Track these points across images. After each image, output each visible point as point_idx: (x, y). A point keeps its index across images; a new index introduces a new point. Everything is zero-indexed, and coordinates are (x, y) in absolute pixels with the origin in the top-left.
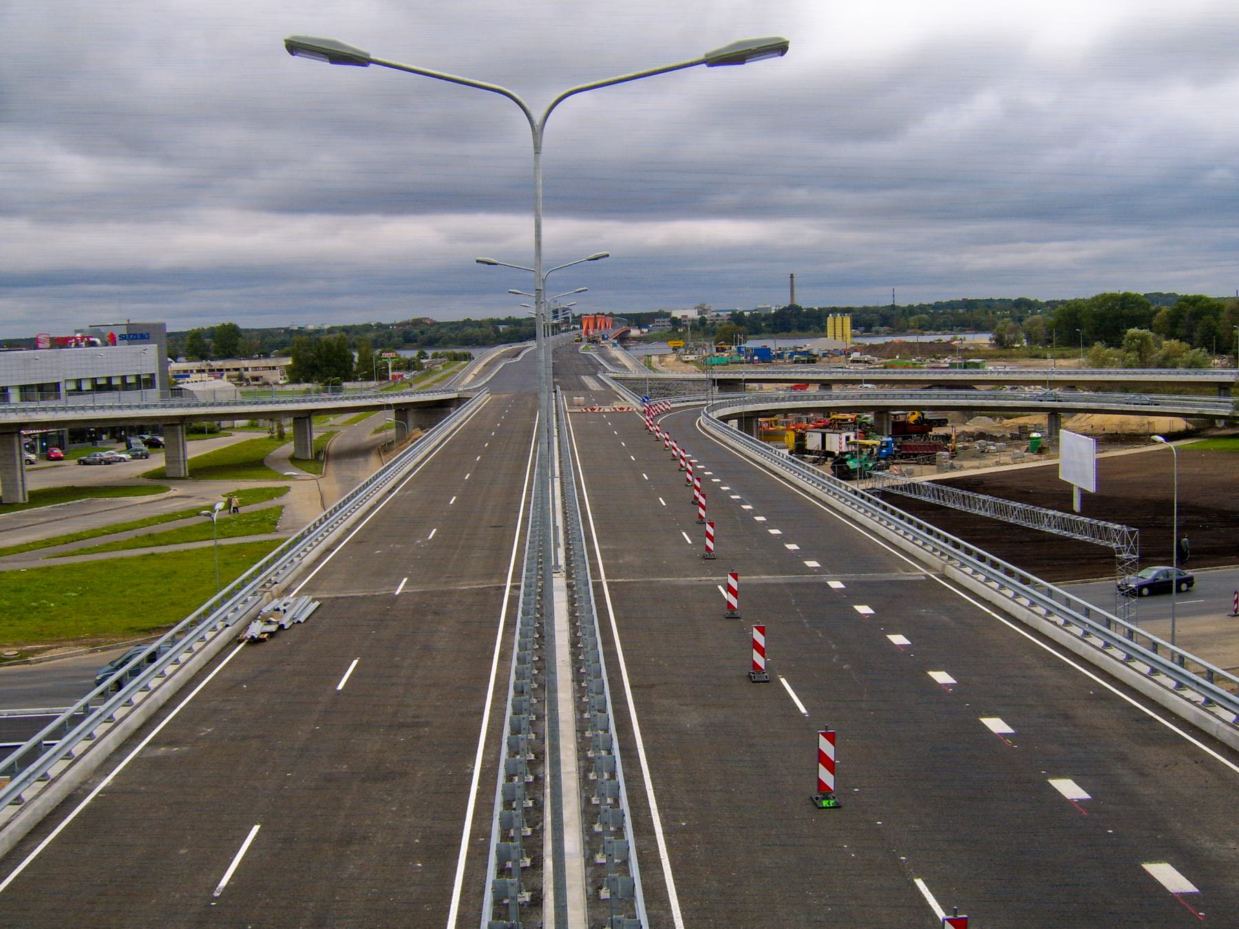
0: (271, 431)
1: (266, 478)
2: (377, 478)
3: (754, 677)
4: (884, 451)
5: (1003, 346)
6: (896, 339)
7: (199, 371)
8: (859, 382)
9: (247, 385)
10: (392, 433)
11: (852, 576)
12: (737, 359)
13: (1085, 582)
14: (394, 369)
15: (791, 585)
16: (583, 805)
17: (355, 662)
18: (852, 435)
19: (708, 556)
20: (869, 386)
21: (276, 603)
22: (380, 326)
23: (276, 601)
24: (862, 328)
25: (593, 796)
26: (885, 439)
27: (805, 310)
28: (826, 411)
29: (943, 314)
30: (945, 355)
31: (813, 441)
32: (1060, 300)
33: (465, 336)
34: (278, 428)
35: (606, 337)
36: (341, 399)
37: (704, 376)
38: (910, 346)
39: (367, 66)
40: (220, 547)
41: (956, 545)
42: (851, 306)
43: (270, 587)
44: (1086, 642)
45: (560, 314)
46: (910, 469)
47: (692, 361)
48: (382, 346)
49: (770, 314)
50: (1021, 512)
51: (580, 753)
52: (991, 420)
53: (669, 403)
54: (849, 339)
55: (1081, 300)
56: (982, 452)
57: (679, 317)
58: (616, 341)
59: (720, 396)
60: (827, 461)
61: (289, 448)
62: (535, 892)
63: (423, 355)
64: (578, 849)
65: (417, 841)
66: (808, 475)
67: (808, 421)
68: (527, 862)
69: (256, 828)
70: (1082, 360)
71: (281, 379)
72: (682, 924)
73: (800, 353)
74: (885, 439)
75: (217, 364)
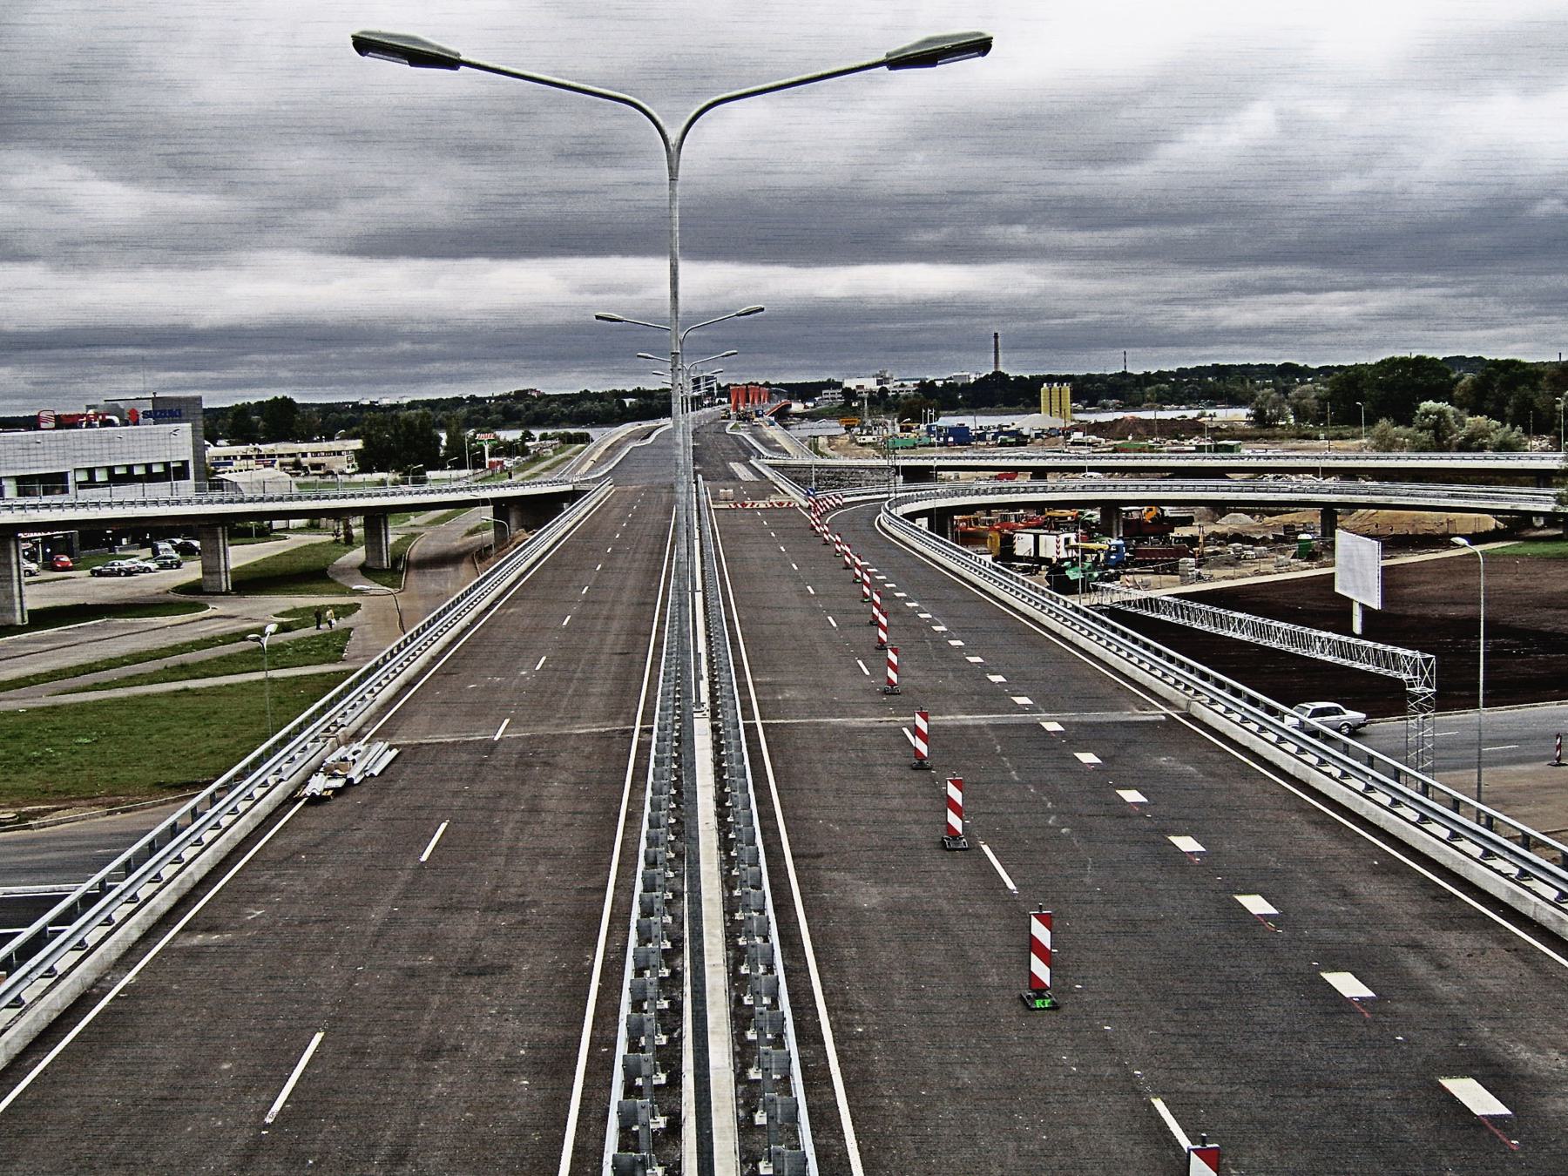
0: (336, 533)
4: (1113, 557)
5: (1264, 427)
7: (244, 457)
8: (1081, 469)
10: (491, 533)
12: (926, 440)
14: (491, 455)
15: (995, 727)
18: (1072, 536)
19: (890, 690)
21: (342, 751)
23: (343, 748)
31: (1023, 545)
35: (760, 413)
40: (272, 680)
41: (1204, 676)
43: (336, 731)
47: (869, 443)
57: (853, 388)
59: (904, 488)
61: (358, 554)
65: (522, 1052)
68: (662, 1078)
73: (1006, 433)
74: (1114, 541)
75: (266, 448)
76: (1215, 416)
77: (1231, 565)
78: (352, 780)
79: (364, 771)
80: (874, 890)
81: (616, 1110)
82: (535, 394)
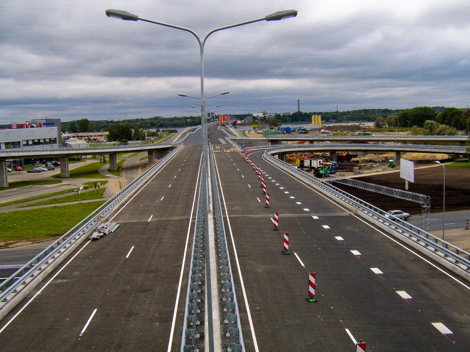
0: (101, 160)
1: (99, 177)
4: (334, 167)
5: (379, 127)
6: (338, 124)
8: (324, 141)
11: (322, 214)
12: (278, 132)
14: (147, 136)
16: (220, 301)
18: (321, 161)
19: (267, 207)
21: (103, 225)
22: (142, 119)
23: (103, 224)
24: (326, 120)
25: (223, 298)
26: (334, 162)
27: (303, 113)
28: (312, 152)
30: (357, 130)
31: (307, 163)
35: (228, 124)
37: (265, 138)
38: (344, 127)
40: (82, 204)
43: (101, 219)
49: (291, 115)
56: (371, 167)
57: (256, 116)
61: (108, 166)
64: (218, 318)
65: (157, 315)
66: (305, 176)
67: (305, 156)
68: (198, 323)
69: (96, 310)
70: (409, 132)
71: (104, 140)
72: (257, 346)
73: (302, 130)
74: (334, 162)
75: (80, 134)
76: (364, 125)
80: (262, 267)
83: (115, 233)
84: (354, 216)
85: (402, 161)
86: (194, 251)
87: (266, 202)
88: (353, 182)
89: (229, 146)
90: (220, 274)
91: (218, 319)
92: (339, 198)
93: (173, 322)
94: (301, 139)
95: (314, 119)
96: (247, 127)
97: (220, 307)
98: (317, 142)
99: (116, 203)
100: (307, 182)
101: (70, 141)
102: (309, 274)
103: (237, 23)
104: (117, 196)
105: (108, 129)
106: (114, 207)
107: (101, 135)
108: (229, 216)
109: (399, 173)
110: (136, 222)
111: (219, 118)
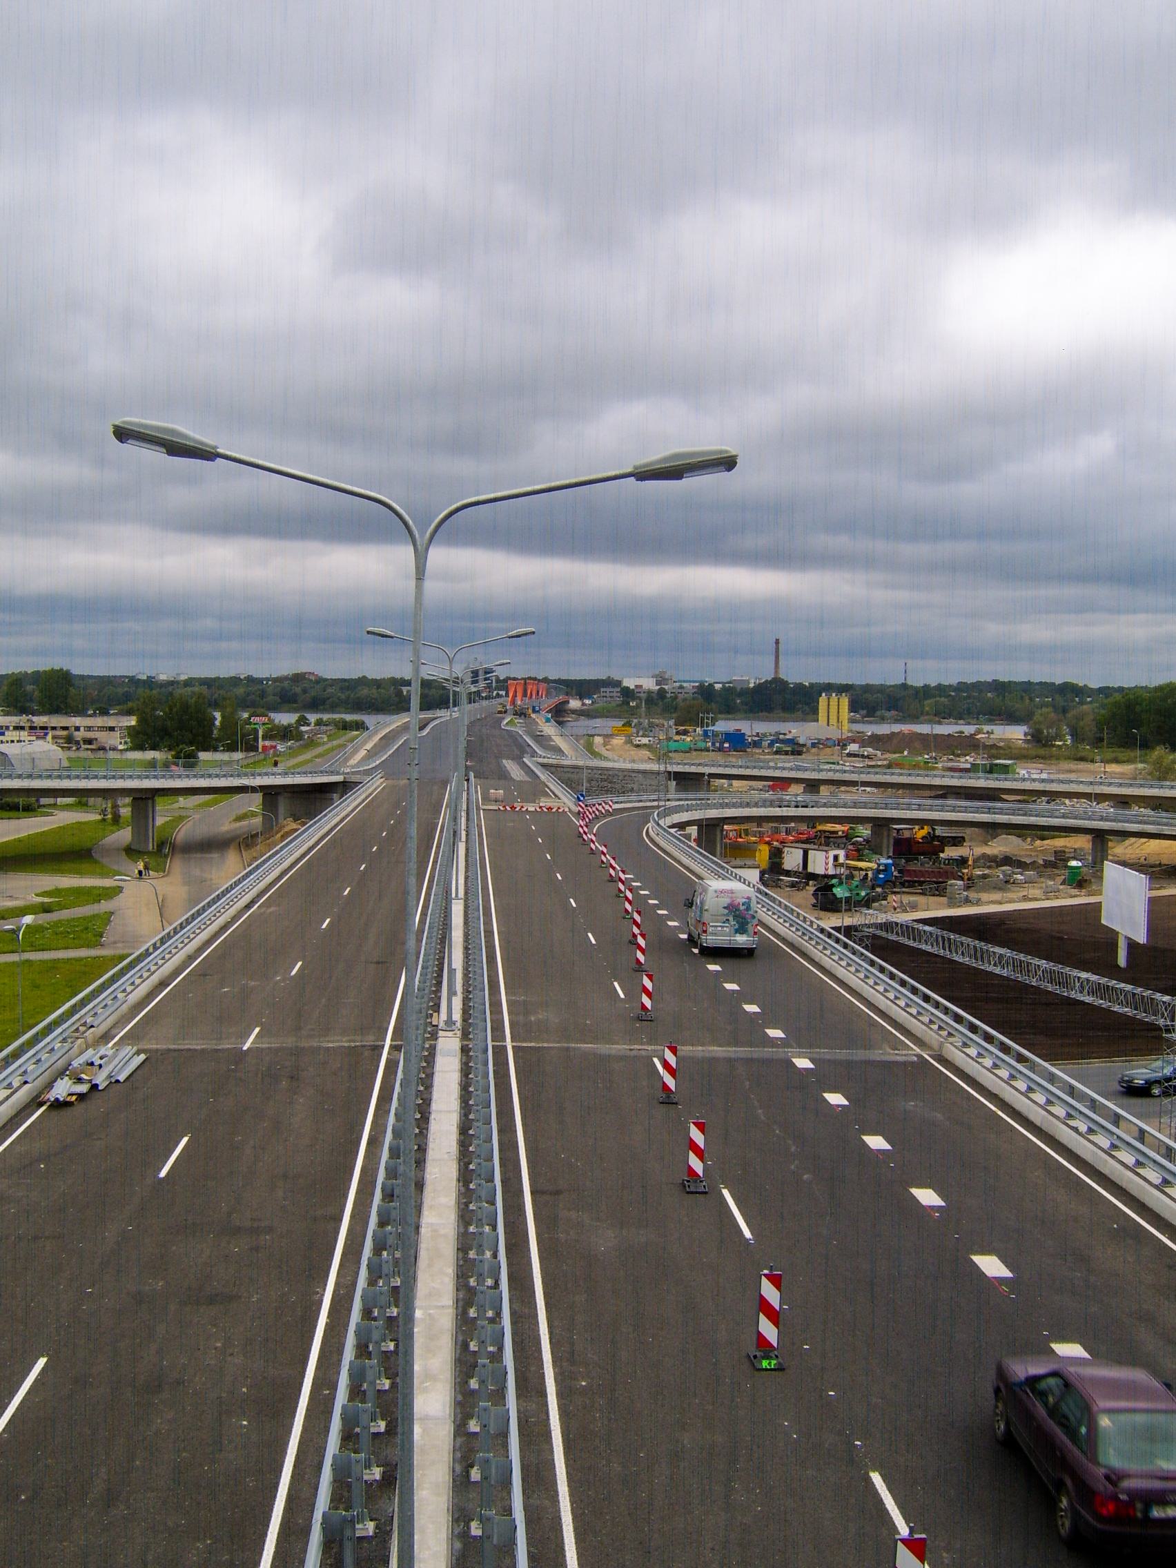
0: (104, 812)
1: (93, 874)
2: (232, 889)
3: (689, 1186)
4: (881, 876)
5: (1040, 746)
6: (906, 728)
7: (17, 728)
8: (853, 783)
9: (78, 749)
10: (258, 821)
11: (825, 1053)
12: (701, 745)
13: (1126, 1061)
14: (264, 738)
15: (749, 1061)
16: (458, 1351)
17: (185, 1140)
18: (841, 854)
19: (644, 1016)
20: (868, 789)
21: (89, 1054)
22: (250, 680)
23: (90, 1052)
24: (864, 712)
25: (471, 1341)
26: (883, 861)
27: (792, 686)
28: (812, 821)
29: (965, 698)
30: (966, 752)
31: (792, 859)
32: (1116, 686)
33: (358, 698)
34: (112, 808)
35: (537, 709)
36: (195, 776)
37: (654, 767)
38: (924, 738)
39: (214, 461)
40: (28, 962)
41: (958, 1019)
42: (851, 683)
43: (85, 1032)
44: (1113, 1157)
45: (481, 677)
46: (913, 901)
47: (645, 745)
48: (253, 705)
49: (749, 688)
50: (1047, 971)
51: (460, 1280)
52: (1019, 841)
53: (610, 803)
54: (846, 725)
55: (1142, 687)
56: (1006, 882)
57: (632, 687)
58: (550, 716)
59: (677, 796)
60: (808, 884)
61: (124, 835)
62: (388, 1468)
63: (303, 721)
64: (448, 1412)
65: (244, 1390)
66: (780, 912)
67: (788, 832)
68: (382, 1426)
69: (42, 1362)
70: (1140, 766)
71: (121, 743)
72: (571, 1521)
73: (782, 742)
74: (883, 861)
75: (40, 720)
76: (992, 733)
77: (1000, 889)
78: (97, 1085)
79: (110, 1076)
80: (610, 1233)
81: (340, 1412)
82: (313, 678)
83: (127, 1084)
84: (933, 1065)
85: (1111, 870)
86: (386, 1169)
87: (643, 1001)
88: (940, 939)
89: (536, 790)
90: (468, 1253)
91: (447, 1417)
92: (887, 998)
93: (310, 1388)
94: (777, 774)
95: (826, 707)
96: (598, 722)
97: (457, 1374)
98: (832, 788)
99: (141, 977)
100: (786, 932)
101: (4, 740)
102: (763, 1277)
103: (539, 483)
104: (154, 948)
105: (135, 705)
106: (132, 991)
107: (110, 727)
108: (514, 1044)
109: (1097, 907)
110: (203, 1050)
111: (507, 687)
